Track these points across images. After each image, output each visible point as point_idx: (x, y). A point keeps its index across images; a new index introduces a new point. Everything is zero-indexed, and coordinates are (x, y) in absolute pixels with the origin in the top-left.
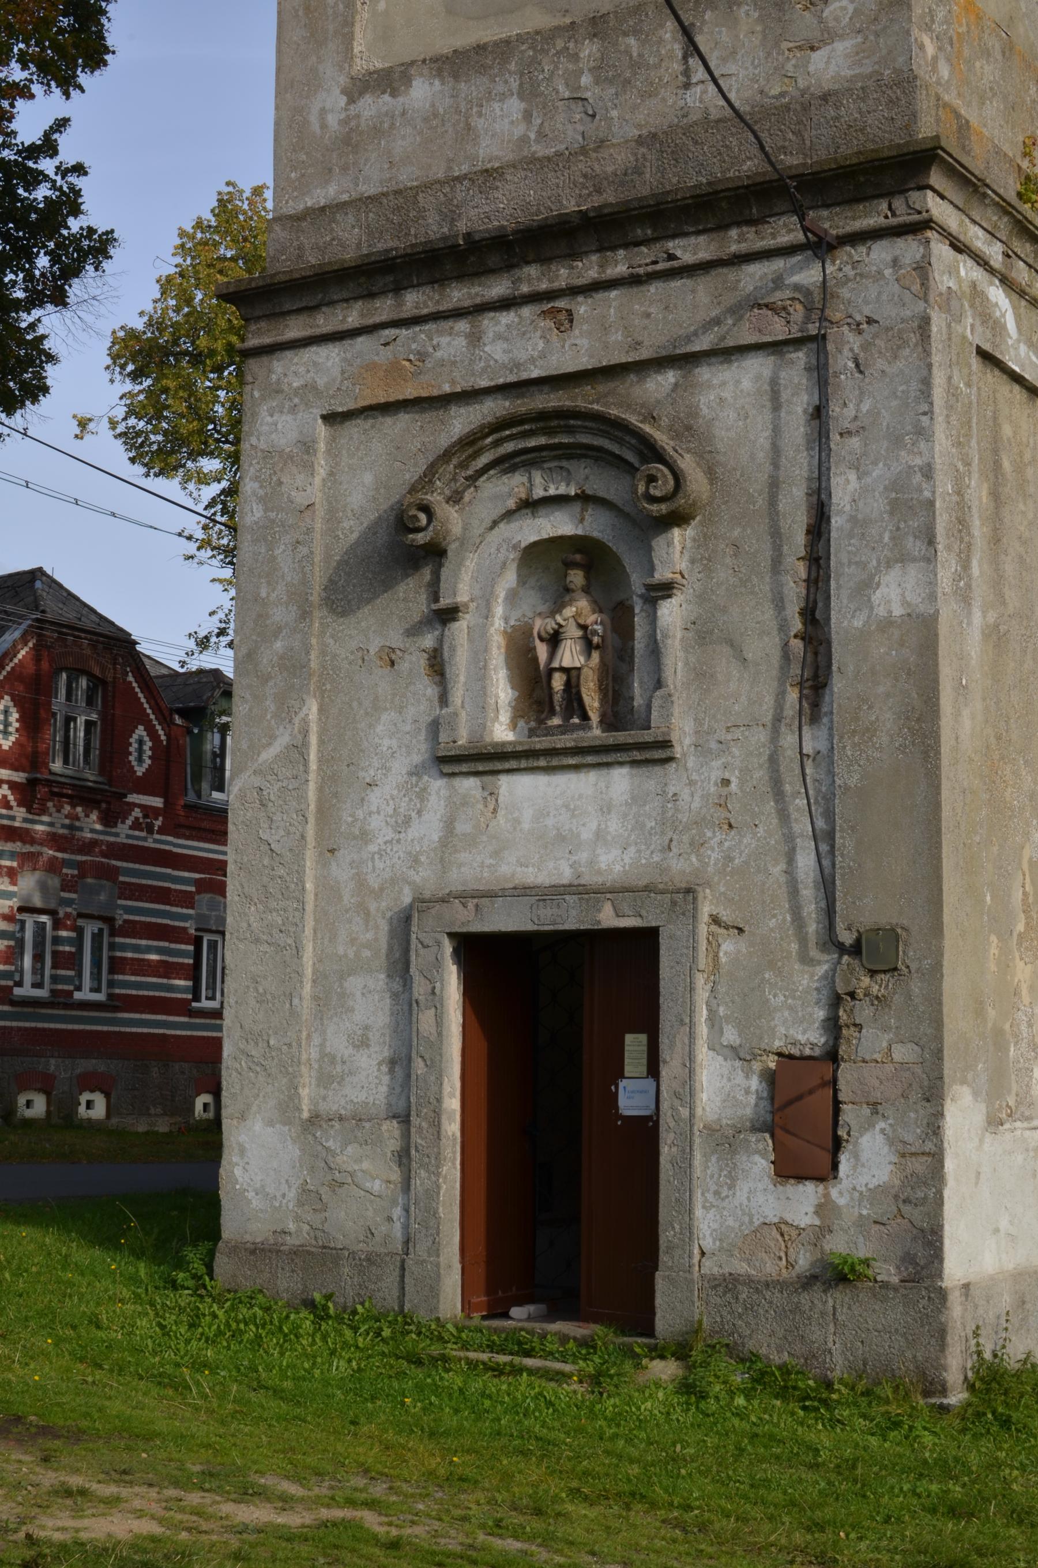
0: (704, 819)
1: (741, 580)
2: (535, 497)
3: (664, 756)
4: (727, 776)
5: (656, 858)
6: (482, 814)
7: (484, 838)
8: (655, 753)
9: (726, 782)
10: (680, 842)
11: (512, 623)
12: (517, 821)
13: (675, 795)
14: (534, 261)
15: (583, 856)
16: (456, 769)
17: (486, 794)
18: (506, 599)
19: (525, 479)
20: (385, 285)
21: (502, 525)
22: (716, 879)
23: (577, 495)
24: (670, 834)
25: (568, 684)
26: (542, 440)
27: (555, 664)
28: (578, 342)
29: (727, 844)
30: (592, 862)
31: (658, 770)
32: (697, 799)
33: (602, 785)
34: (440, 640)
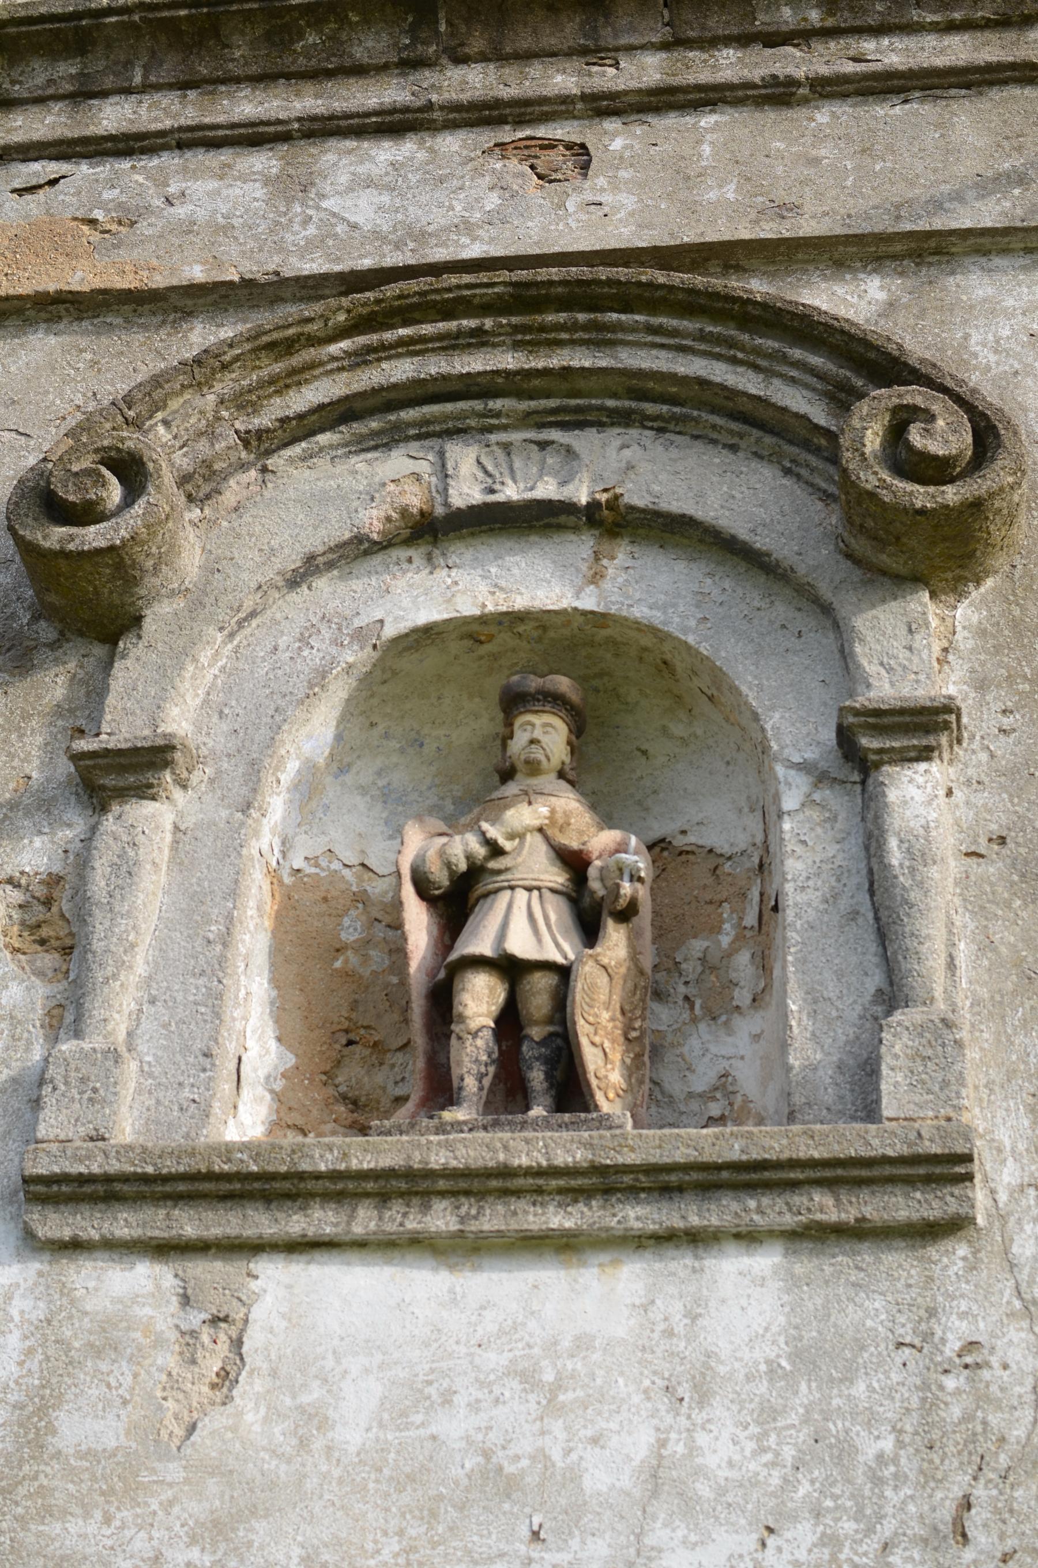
2: (458, 501)
6: (173, 1383)
7: (174, 1471)
11: (298, 863)
12: (318, 1417)
14: (483, 58)
16: (88, 1224)
17: (196, 1318)
18: (295, 787)
19: (424, 467)
20: (51, 82)
21: (322, 583)
23: (593, 506)
24: (959, 1483)
25: (509, 1022)
26: (509, 360)
28: (605, 198)
31: (898, 1264)
33: (671, 1306)
34: (81, 860)
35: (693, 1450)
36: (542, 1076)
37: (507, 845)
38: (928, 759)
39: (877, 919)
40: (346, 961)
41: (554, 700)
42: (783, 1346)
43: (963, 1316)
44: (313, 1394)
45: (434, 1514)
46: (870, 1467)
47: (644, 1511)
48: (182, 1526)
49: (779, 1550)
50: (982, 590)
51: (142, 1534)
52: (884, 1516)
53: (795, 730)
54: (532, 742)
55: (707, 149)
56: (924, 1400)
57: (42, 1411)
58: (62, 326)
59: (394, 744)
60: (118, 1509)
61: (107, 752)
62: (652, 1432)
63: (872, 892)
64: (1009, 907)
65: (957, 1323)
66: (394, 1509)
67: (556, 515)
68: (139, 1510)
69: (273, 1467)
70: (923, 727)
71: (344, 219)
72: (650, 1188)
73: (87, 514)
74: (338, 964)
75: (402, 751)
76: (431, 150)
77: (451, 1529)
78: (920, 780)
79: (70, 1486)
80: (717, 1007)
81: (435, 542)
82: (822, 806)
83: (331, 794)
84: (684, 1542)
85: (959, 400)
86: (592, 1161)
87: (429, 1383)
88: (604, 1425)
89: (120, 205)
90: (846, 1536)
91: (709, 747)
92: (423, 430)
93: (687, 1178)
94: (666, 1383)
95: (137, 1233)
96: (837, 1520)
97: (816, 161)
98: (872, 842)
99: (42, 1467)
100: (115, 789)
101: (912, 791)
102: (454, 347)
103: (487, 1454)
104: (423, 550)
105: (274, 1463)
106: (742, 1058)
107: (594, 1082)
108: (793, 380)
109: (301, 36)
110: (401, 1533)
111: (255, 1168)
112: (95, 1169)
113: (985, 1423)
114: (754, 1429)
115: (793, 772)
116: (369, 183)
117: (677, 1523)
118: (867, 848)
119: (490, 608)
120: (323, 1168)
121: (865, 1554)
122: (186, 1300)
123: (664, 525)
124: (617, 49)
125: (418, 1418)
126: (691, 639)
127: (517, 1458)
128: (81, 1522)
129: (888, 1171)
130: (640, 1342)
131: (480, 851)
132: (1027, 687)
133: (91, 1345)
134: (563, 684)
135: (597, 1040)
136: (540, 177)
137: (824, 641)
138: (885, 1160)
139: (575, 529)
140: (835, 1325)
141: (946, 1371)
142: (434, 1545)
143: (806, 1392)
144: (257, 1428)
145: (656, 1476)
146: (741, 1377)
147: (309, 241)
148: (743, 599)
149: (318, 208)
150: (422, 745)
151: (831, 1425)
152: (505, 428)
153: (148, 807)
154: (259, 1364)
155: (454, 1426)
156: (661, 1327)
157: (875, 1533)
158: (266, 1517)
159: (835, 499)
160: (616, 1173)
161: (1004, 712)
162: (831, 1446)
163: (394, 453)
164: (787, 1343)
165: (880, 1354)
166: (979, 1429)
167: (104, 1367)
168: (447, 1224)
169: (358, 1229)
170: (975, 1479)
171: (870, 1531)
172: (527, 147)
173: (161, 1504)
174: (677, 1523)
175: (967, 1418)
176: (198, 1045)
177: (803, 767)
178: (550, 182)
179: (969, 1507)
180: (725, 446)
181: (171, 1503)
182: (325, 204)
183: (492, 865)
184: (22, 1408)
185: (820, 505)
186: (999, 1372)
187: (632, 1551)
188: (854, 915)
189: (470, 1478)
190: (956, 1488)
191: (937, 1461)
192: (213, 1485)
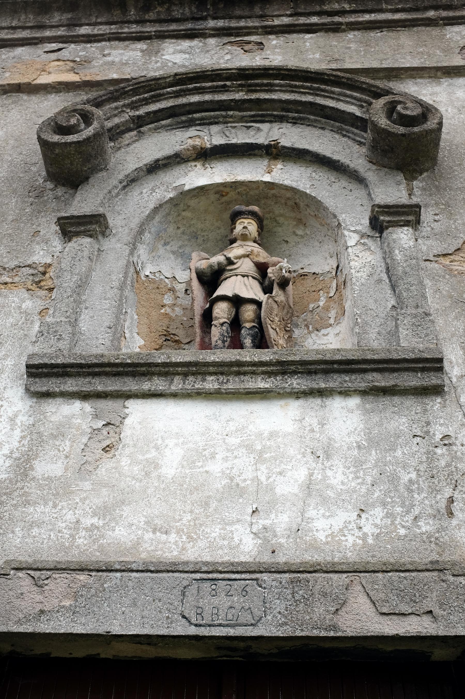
5: (426, 526)
7: (87, 485)
17: (100, 424)
24: (448, 492)
31: (410, 402)
35: (325, 478)
36: (250, 341)
39: (390, 281)
40: (166, 311)
41: (253, 214)
42: (363, 436)
43: (441, 425)
44: (153, 454)
45: (207, 504)
46: (406, 485)
47: (304, 503)
48: (90, 508)
50: (423, 176)
51: (71, 512)
52: (415, 505)
56: (428, 458)
57: (28, 460)
58: (61, 94)
59: (186, 237)
60: (60, 501)
61: (72, 217)
62: (306, 470)
65: (440, 428)
66: (189, 502)
67: (254, 150)
68: (70, 502)
69: (133, 484)
72: (302, 372)
74: (162, 311)
75: (189, 240)
76: (204, 43)
77: (215, 510)
78: (406, 232)
79: (38, 492)
82: (364, 244)
83: (161, 252)
84: (323, 516)
86: (277, 359)
87: (205, 450)
88: (285, 467)
89: (86, 56)
90: (398, 514)
92: (202, 122)
93: (319, 367)
94: (311, 450)
95: (75, 389)
96: (393, 507)
97: (350, 48)
99: (26, 484)
102: (215, 92)
103: (232, 479)
105: (134, 482)
106: (331, 343)
109: (156, 8)
110: (191, 512)
111: (129, 361)
112: (59, 361)
113: (456, 467)
114: (352, 469)
115: (352, 233)
116: (181, 52)
117: (320, 508)
120: (159, 361)
121: (407, 521)
123: (296, 155)
124: (273, 16)
125: (200, 464)
126: (308, 191)
128: (42, 507)
130: (299, 434)
131: (225, 262)
132: (443, 207)
133: (52, 434)
134: (255, 208)
135: (273, 326)
137: (361, 193)
139: (261, 156)
141: (436, 447)
142: (207, 517)
143: (374, 455)
145: (309, 487)
146: (345, 448)
147: (157, 68)
148: (328, 179)
149: (161, 58)
150: (197, 238)
151: (387, 468)
152: (234, 122)
155: (215, 467)
156: (308, 428)
157: (411, 512)
158: (129, 504)
159: (364, 144)
160: (288, 365)
161: (435, 214)
162: (388, 477)
163: (190, 129)
164: (365, 435)
165: (406, 440)
166: (454, 469)
167: (57, 443)
168: (213, 386)
169: (173, 388)
170: (454, 490)
171: (408, 512)
173: (80, 499)
174: (320, 508)
175: (448, 465)
179: (453, 502)
180: (320, 128)
181: (85, 499)
182: (163, 57)
185: (358, 146)
186: (460, 447)
187: (300, 519)
189: (224, 489)
190: (446, 494)
191: (436, 482)
192: (104, 491)
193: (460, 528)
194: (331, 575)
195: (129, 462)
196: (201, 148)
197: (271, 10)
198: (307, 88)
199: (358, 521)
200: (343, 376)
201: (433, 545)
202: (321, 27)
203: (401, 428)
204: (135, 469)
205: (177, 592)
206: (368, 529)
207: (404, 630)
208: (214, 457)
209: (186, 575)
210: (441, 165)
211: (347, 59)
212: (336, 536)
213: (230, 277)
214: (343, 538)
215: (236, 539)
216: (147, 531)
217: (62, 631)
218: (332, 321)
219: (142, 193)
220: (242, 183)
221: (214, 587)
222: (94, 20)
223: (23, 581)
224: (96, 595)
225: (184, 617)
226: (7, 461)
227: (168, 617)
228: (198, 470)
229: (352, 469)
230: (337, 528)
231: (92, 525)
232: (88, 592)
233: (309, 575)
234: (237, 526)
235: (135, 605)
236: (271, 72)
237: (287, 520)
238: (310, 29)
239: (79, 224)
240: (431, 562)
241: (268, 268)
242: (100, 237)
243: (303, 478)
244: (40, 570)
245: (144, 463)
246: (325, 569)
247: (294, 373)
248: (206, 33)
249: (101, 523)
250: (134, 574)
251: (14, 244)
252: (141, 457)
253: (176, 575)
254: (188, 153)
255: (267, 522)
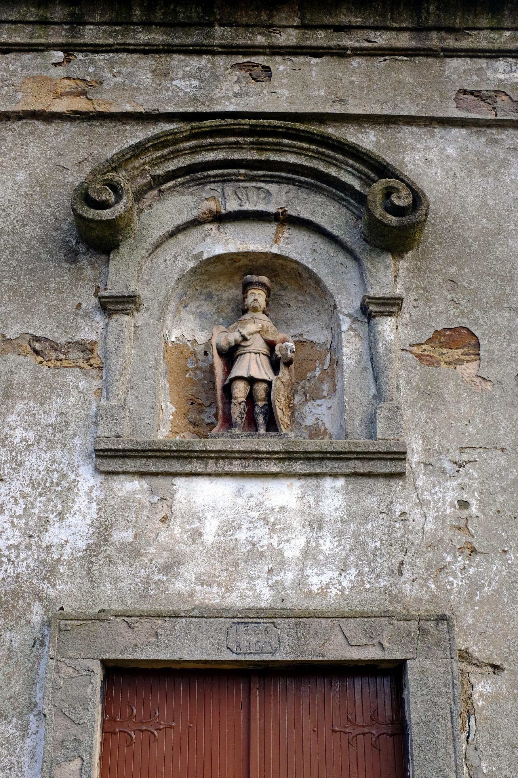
0: (441, 541)
1: (462, 311)
3: (393, 470)
4: (465, 497)
5: (383, 582)
8: (375, 463)
9: (464, 504)
10: (413, 566)
11: (173, 339)
13: (403, 514)
15: (289, 576)
17: (156, 499)
22: (462, 609)
25: (251, 399)
27: (232, 375)
29: (472, 570)
30: (301, 583)
31: (380, 484)
32: (430, 519)
35: (318, 545)
37: (248, 337)
38: (391, 316)
43: (400, 504)
44: (197, 524)
45: (237, 564)
49: (345, 576)
51: (143, 570)
53: (348, 302)
54: (255, 300)
55: (314, 73)
56: (389, 531)
59: (203, 297)
63: (372, 362)
64: (416, 369)
70: (391, 305)
71: (182, 90)
73: (104, 205)
75: (205, 300)
78: (389, 323)
80: (313, 396)
81: (220, 223)
82: (354, 330)
85: (408, 185)
87: (234, 521)
88: (290, 536)
90: (366, 573)
91: (311, 305)
96: (363, 568)
98: (372, 345)
100: (115, 310)
101: (386, 327)
103: (254, 545)
104: (216, 225)
107: (281, 422)
108: (349, 172)
110: (227, 570)
113: (408, 538)
118: (370, 346)
119: (241, 250)
122: (152, 492)
125: (231, 533)
126: (310, 266)
127: (263, 546)
129: (380, 456)
131: (240, 339)
134: (264, 279)
135: (281, 407)
136: (254, 79)
138: (379, 453)
140: (362, 506)
144: (178, 535)
149: (172, 84)
153: (126, 318)
154: (177, 514)
155: (242, 536)
156: (307, 505)
158: (183, 564)
166: (406, 540)
167: (126, 515)
172: (248, 66)
175: (403, 536)
176: (149, 404)
177: (349, 315)
178: (257, 81)
179: (403, 564)
182: (174, 83)
183: (243, 344)
184: (100, 528)
186: (412, 522)
187: (300, 576)
188: (365, 369)
193: (405, 584)
194: (321, 620)
195: (180, 530)
196: (217, 212)
197: (280, 18)
198: (313, 151)
199: (339, 578)
200: (333, 463)
201: (387, 596)
202: (326, 51)
203: (372, 505)
204: (185, 536)
205: (223, 632)
206: (346, 584)
207: (364, 656)
208: (241, 528)
209: (228, 620)
210: (424, 243)
211: (351, 100)
212: (325, 589)
213: (244, 354)
214: (329, 590)
215: (258, 591)
216: (198, 585)
217: (151, 658)
218: (325, 394)
219: (165, 260)
220: (254, 253)
221: (246, 628)
222: (98, 19)
223: (120, 625)
224: (170, 634)
225: (228, 648)
226: (90, 530)
227: (218, 649)
228: (230, 538)
229: (337, 538)
230: (325, 583)
231: (159, 580)
232: (165, 632)
233: (307, 619)
234: (258, 581)
235: (197, 641)
236: (280, 130)
237: (292, 576)
238: (316, 52)
239: (117, 303)
240: (384, 612)
241: (275, 345)
242: (135, 313)
243: (303, 545)
244: (130, 616)
245: (191, 531)
246: (317, 616)
247: (299, 459)
248: (214, 51)
249: (165, 579)
250: (194, 619)
251: (61, 317)
252: (188, 527)
253: (221, 619)
254: (205, 216)
255: (279, 578)
